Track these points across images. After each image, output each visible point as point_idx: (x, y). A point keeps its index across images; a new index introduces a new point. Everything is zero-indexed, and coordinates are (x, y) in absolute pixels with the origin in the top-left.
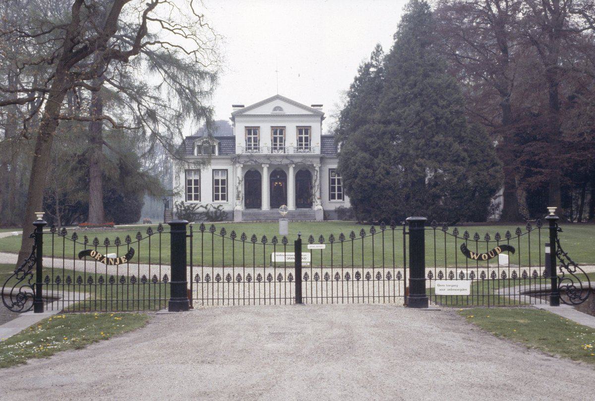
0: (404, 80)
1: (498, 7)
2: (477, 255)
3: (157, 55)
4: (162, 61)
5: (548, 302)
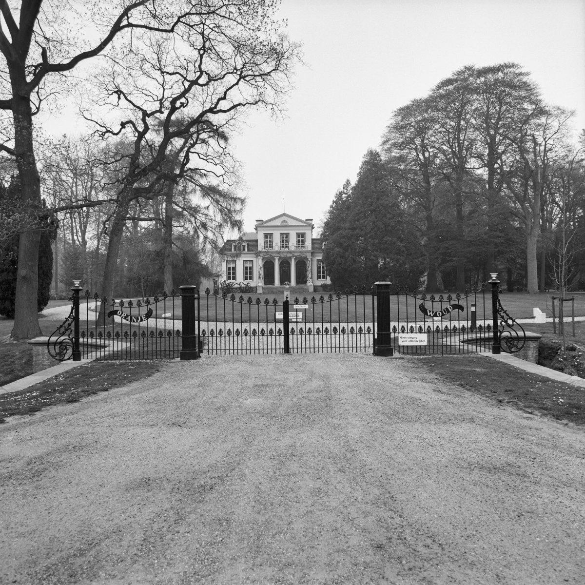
0: (364, 202)
1: (424, 155)
2: (433, 312)
3: (206, 187)
4: (209, 191)
5: (491, 351)
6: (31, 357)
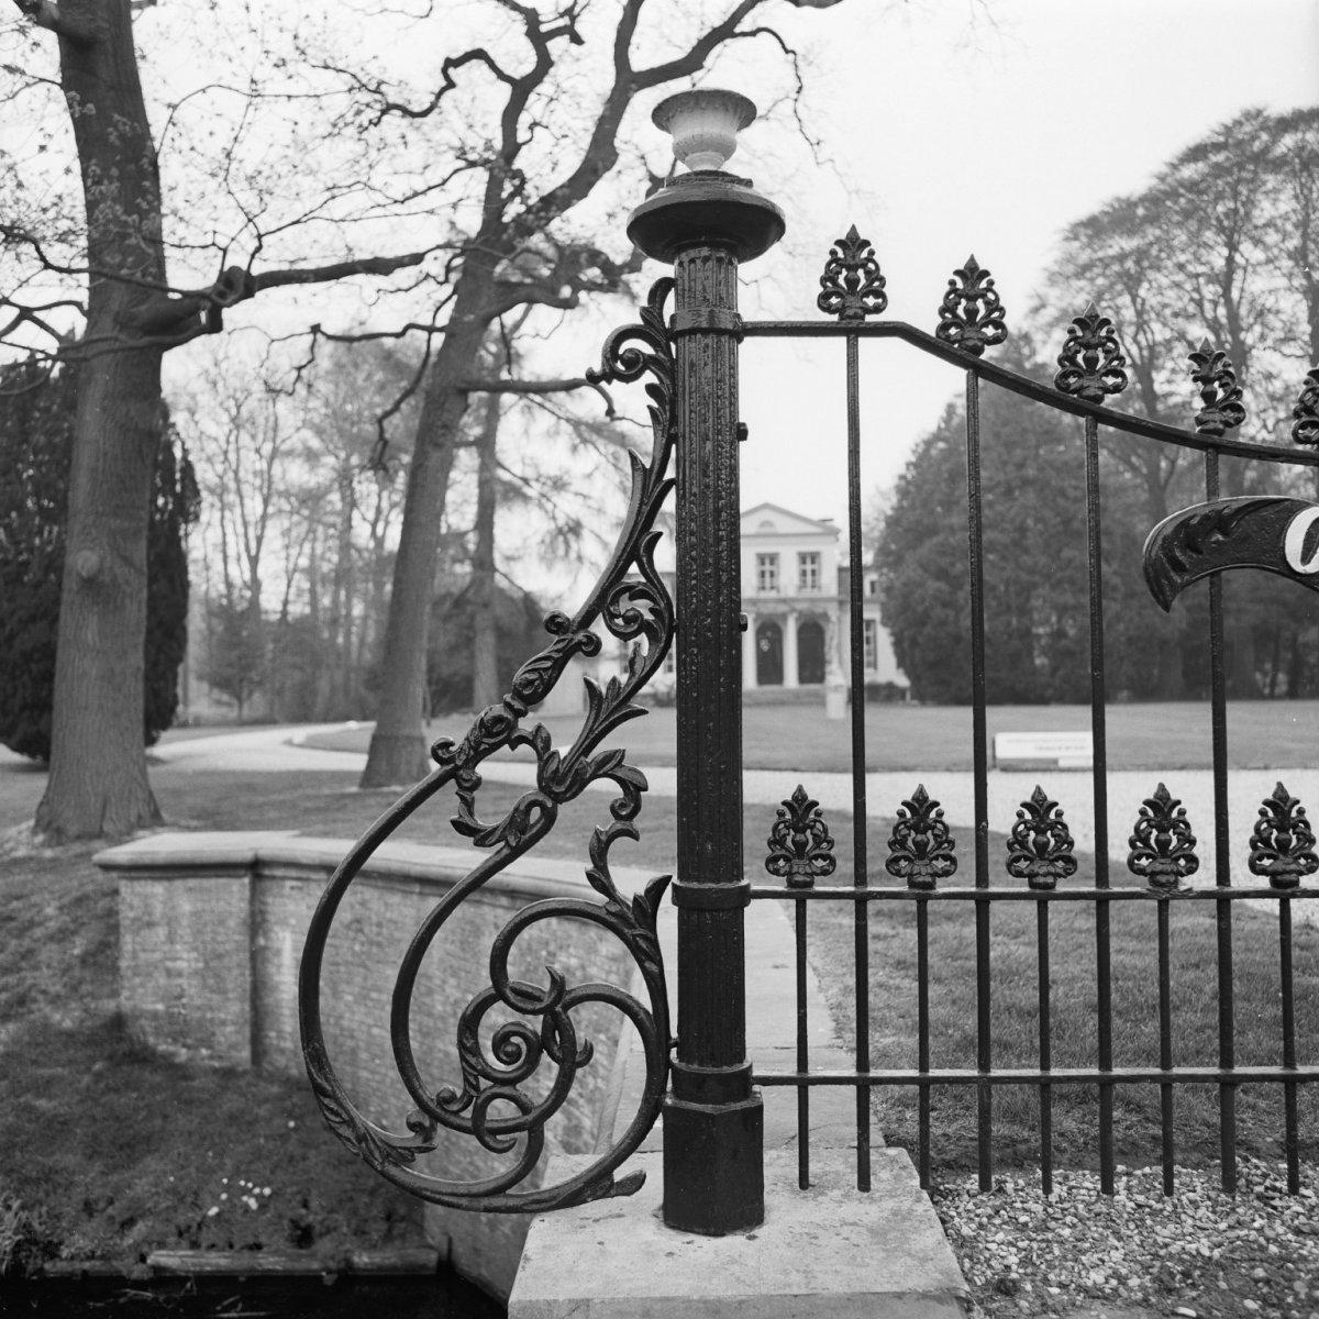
6: (111, 925)
